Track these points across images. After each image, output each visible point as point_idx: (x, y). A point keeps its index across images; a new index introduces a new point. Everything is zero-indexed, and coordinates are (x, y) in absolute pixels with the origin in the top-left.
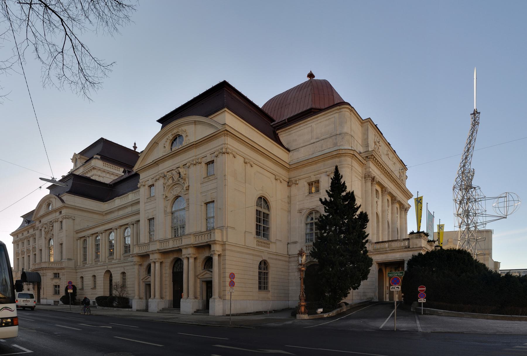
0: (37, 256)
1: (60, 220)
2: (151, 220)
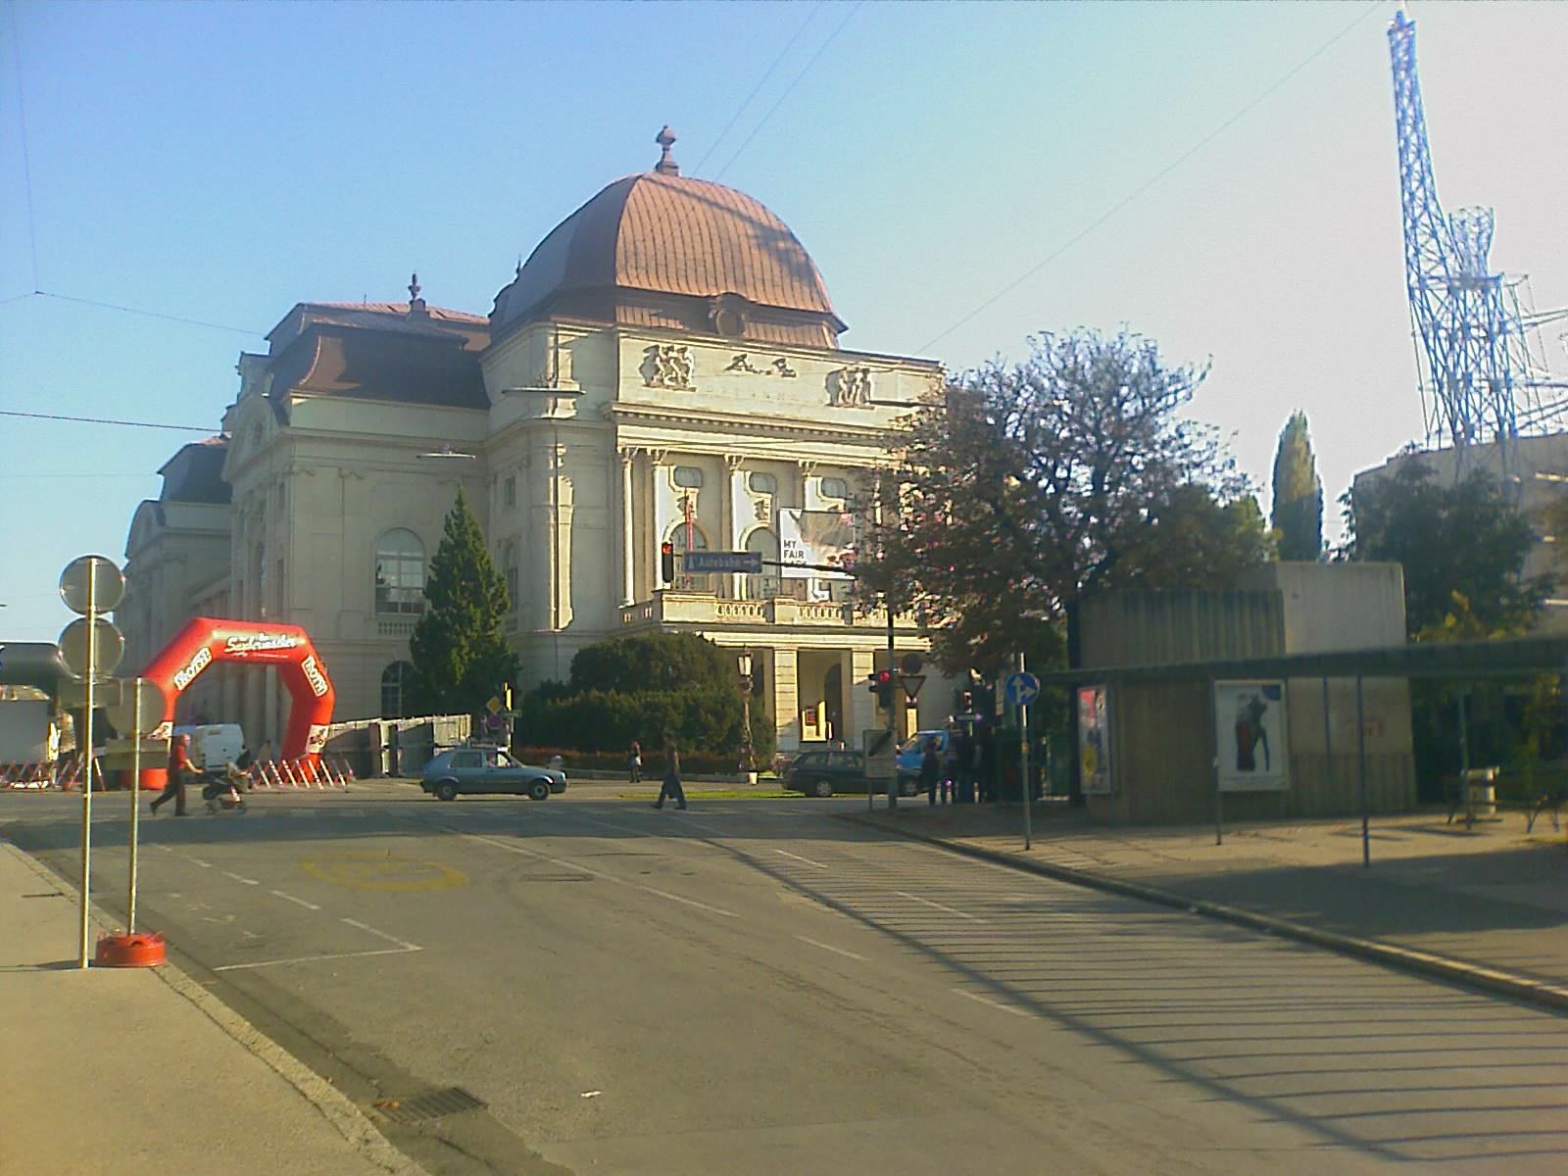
0: (245, 588)
1: (279, 481)
2: (241, 583)
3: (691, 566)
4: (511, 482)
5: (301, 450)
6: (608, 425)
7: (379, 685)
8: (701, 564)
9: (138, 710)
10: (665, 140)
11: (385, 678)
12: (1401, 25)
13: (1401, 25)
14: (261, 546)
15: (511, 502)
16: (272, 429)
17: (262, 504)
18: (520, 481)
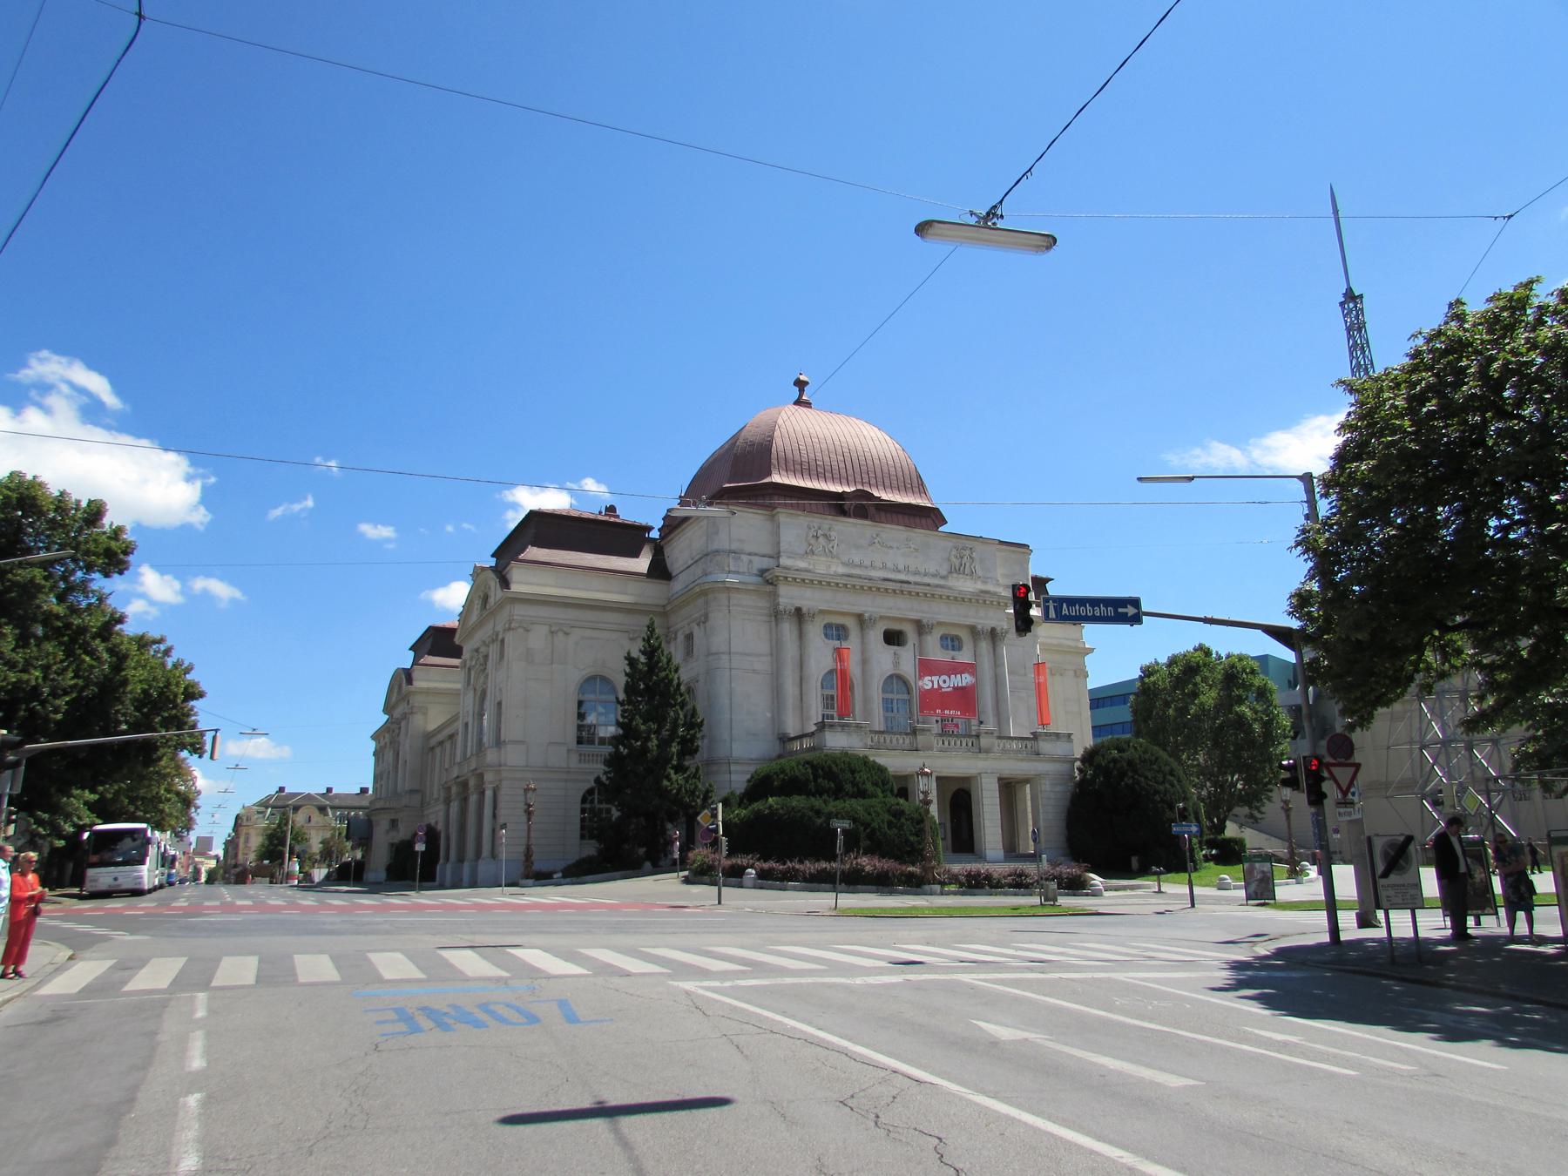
3: (1052, 614)
4: (689, 637)
5: (520, 611)
6: (769, 588)
7: (578, 806)
8: (1065, 611)
9: (778, 1018)
10: (801, 385)
11: (584, 800)
12: (1351, 297)
13: (1351, 297)
14: (484, 693)
15: (689, 652)
16: (496, 593)
17: (486, 657)
18: (698, 633)
